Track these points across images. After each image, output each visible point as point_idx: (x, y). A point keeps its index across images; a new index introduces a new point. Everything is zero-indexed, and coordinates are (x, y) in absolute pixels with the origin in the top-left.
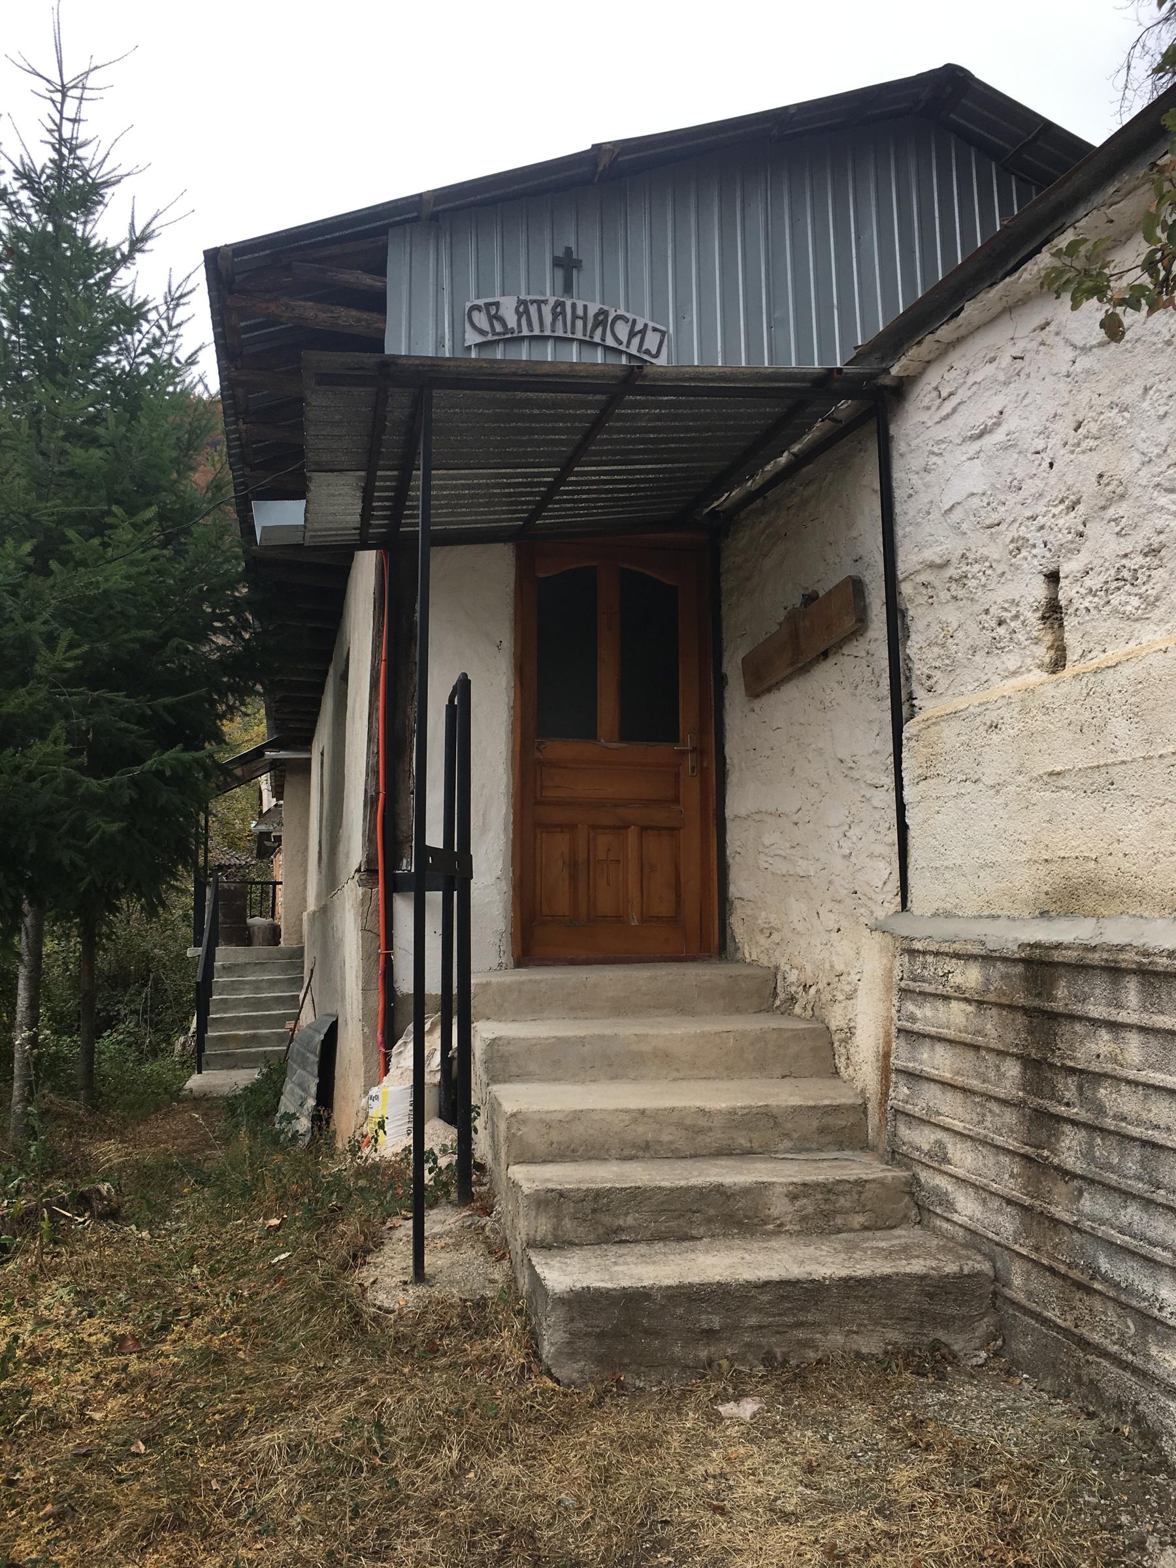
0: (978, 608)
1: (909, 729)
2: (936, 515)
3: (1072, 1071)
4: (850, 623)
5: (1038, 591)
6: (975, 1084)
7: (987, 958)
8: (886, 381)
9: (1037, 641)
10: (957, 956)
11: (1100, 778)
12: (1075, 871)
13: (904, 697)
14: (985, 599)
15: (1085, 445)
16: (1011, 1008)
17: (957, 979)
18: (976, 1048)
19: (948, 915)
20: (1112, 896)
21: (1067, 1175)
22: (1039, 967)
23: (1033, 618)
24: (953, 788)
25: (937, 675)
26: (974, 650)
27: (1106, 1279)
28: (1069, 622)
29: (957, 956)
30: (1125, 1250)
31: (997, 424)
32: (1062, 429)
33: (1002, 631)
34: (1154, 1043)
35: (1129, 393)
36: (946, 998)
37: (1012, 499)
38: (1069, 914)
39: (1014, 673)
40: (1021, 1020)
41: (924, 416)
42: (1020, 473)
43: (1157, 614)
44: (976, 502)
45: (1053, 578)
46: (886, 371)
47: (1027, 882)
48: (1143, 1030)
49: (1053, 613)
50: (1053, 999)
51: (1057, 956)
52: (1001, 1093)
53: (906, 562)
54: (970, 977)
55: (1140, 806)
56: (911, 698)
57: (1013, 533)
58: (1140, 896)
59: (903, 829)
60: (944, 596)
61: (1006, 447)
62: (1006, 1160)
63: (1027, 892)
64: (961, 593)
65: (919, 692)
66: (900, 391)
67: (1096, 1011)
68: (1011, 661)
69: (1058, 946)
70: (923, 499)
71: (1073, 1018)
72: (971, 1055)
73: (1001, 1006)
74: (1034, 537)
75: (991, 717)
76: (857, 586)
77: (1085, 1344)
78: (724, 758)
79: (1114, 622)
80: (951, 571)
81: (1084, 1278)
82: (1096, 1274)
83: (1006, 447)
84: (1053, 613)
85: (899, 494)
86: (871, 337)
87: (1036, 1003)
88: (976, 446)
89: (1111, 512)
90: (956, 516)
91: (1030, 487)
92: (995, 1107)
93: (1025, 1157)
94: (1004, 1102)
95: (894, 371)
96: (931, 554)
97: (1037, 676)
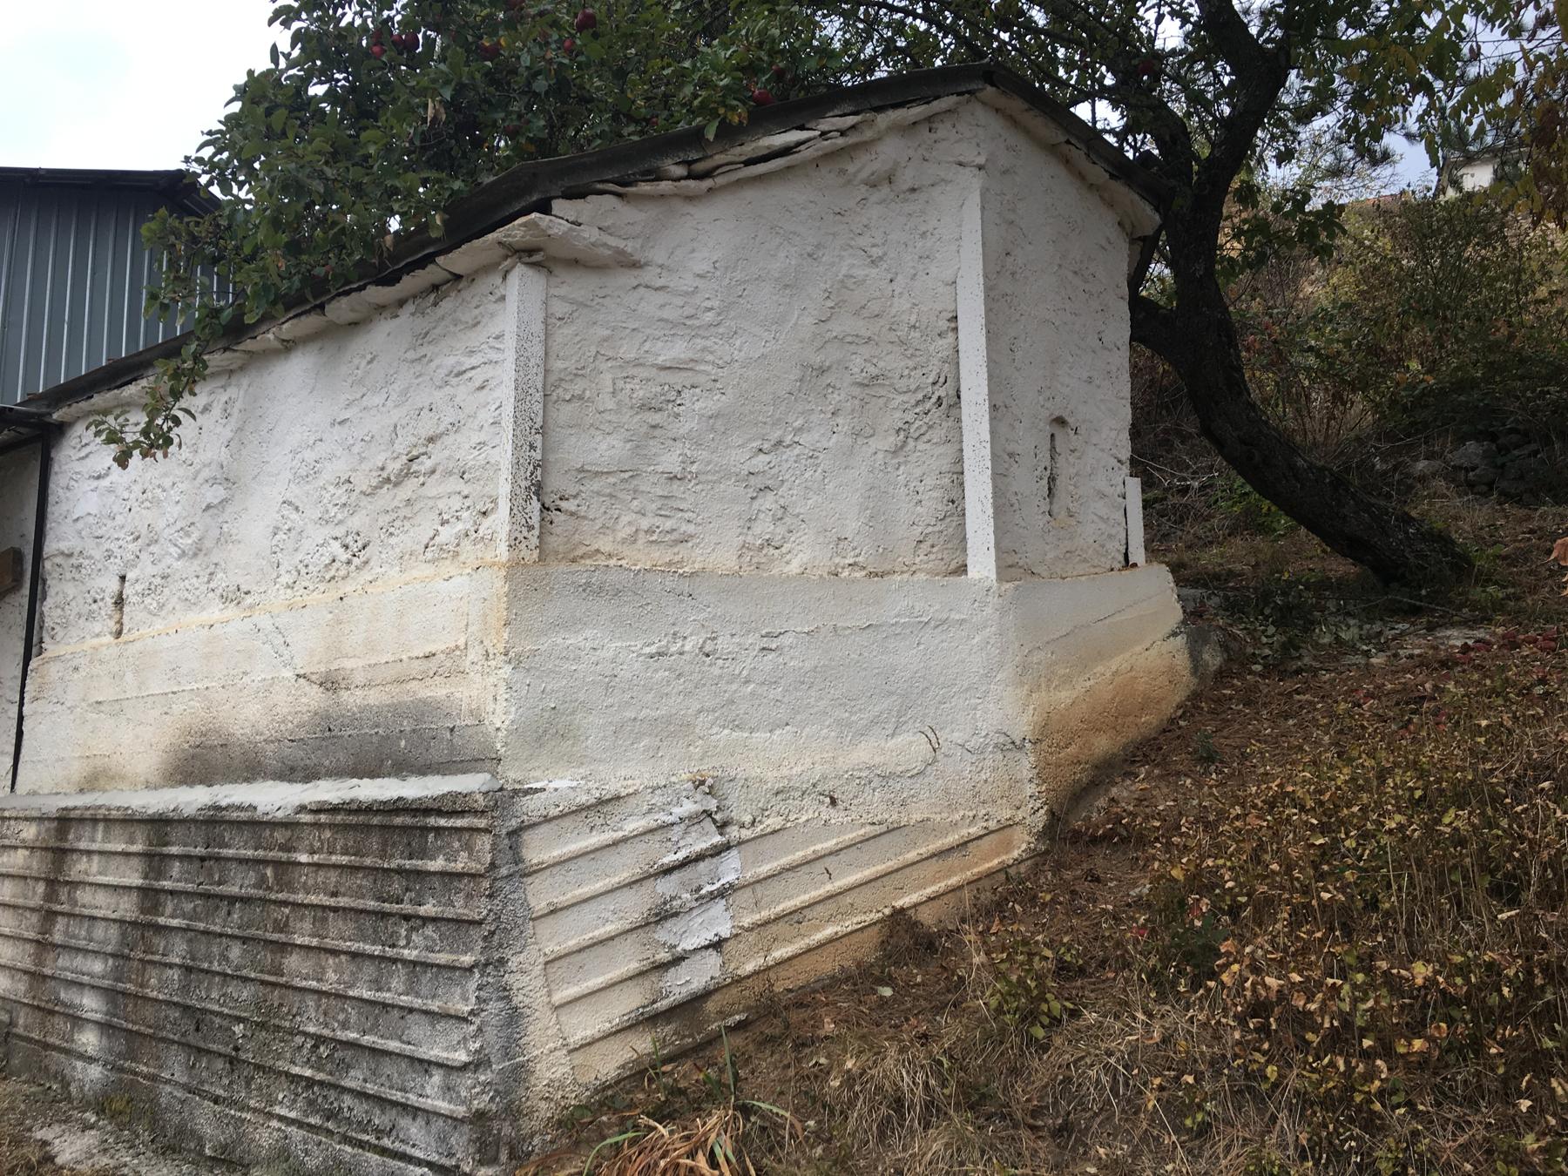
0: (85, 589)
1: (33, 664)
2: (69, 520)
3: (67, 883)
4: (8, 581)
5: (114, 585)
6: (21, 901)
7: (40, 819)
8: (47, 419)
9: (110, 617)
10: (26, 819)
11: (117, 707)
12: (99, 762)
13: (35, 640)
14: (89, 584)
15: (147, 504)
16: (46, 849)
17: (23, 835)
18: (25, 878)
19: (35, 793)
20: (113, 778)
21: (55, 946)
22: (65, 822)
23: (110, 601)
24: (51, 707)
25: (58, 628)
26: (80, 615)
27: (65, 1005)
28: (126, 609)
29: (26, 819)
30: (73, 983)
31: (107, 475)
32: (137, 489)
33: (95, 606)
34: (104, 859)
35: (167, 483)
36: (16, 848)
37: (110, 523)
38: (93, 790)
39: (98, 635)
40: (50, 855)
41: (71, 452)
42: (115, 509)
43: (163, 613)
44: (91, 520)
45: (123, 578)
46: (50, 414)
47: (77, 770)
48: (101, 853)
49: (120, 602)
50: (66, 840)
51: (72, 815)
52: (32, 904)
53: (50, 546)
54: (29, 832)
55: (131, 726)
56: (41, 641)
57: (107, 546)
58: (123, 778)
59: (20, 734)
60: (68, 576)
61: (110, 491)
62: (28, 946)
63: (76, 777)
64: (77, 576)
65: (47, 639)
66: (61, 429)
67: (83, 845)
68: (97, 627)
69: (75, 808)
70: (64, 507)
71: (74, 851)
72: (22, 883)
73: (42, 849)
74: (118, 552)
75: (75, 663)
76: (17, 556)
77: (47, 1046)
78: (424, 774)
79: (145, 613)
80: (73, 561)
81: (50, 1006)
82: (58, 1002)
83: (110, 491)
84: (120, 602)
85: (52, 499)
86: (50, 386)
87: (58, 844)
88: (95, 483)
89: (151, 548)
90: (80, 525)
91: (120, 520)
92: (28, 914)
93: (38, 942)
94: (33, 910)
95: (55, 416)
96: (64, 546)
97: (109, 639)
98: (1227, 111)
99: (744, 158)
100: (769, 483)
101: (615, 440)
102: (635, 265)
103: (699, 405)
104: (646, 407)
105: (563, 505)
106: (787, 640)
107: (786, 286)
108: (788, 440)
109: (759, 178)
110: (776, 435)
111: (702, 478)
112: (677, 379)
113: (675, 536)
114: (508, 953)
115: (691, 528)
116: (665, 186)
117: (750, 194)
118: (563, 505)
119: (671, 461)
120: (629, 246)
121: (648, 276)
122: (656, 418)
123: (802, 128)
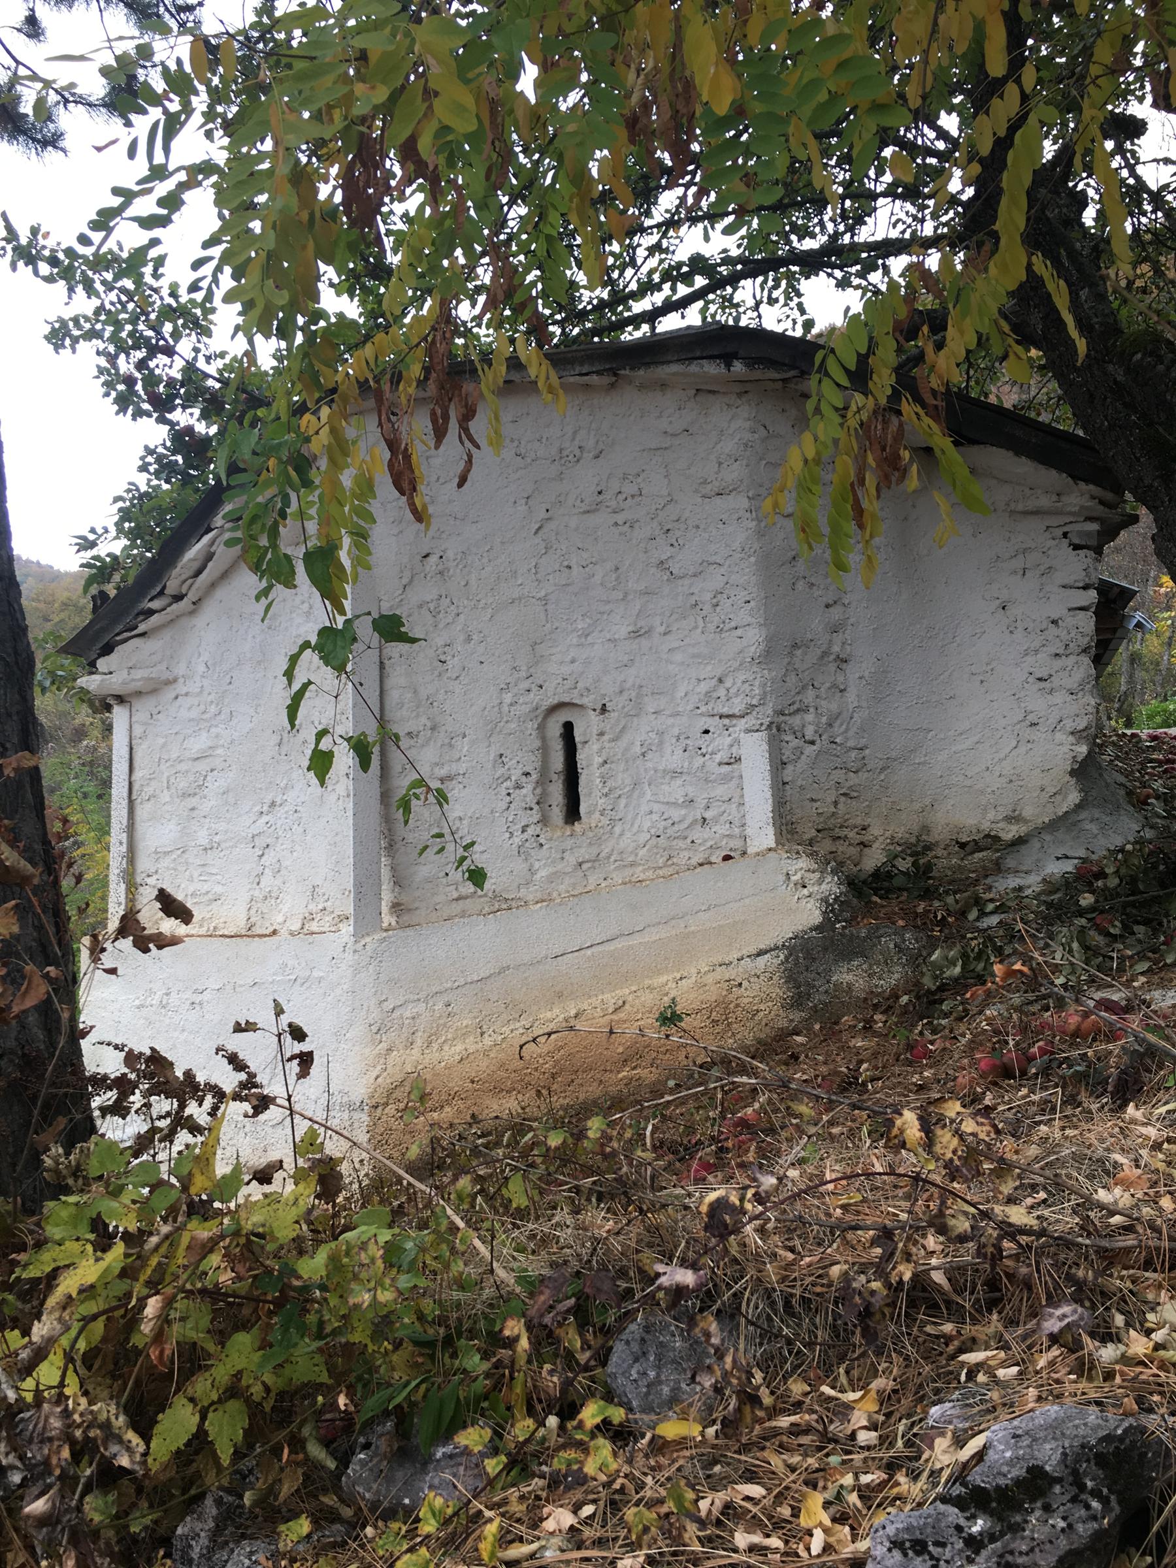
98: (1055, 19)
99: (190, 573)
100: (269, 841)
101: (172, 826)
102: (169, 682)
103: (216, 784)
104: (185, 795)
105: (149, 880)
106: (206, 996)
107: (259, 662)
108: (278, 801)
109: (213, 585)
110: (268, 799)
111: (223, 845)
112: (202, 766)
113: (210, 896)
114: (710, 1178)
115: (219, 889)
116: (154, 620)
117: (220, 593)
118: (149, 880)
119: (203, 838)
120: (154, 673)
121: (180, 688)
122: (193, 801)
123: (207, 532)
